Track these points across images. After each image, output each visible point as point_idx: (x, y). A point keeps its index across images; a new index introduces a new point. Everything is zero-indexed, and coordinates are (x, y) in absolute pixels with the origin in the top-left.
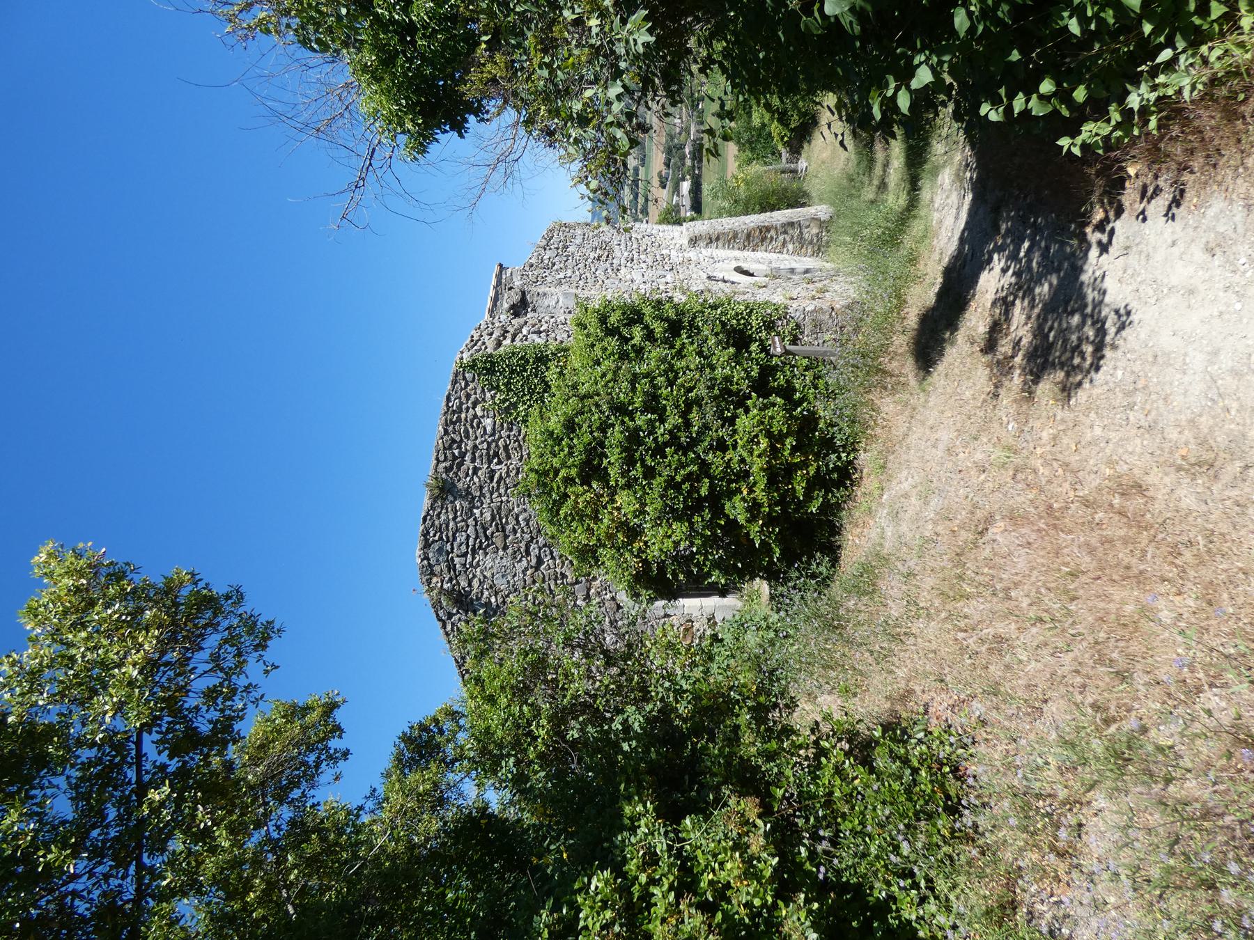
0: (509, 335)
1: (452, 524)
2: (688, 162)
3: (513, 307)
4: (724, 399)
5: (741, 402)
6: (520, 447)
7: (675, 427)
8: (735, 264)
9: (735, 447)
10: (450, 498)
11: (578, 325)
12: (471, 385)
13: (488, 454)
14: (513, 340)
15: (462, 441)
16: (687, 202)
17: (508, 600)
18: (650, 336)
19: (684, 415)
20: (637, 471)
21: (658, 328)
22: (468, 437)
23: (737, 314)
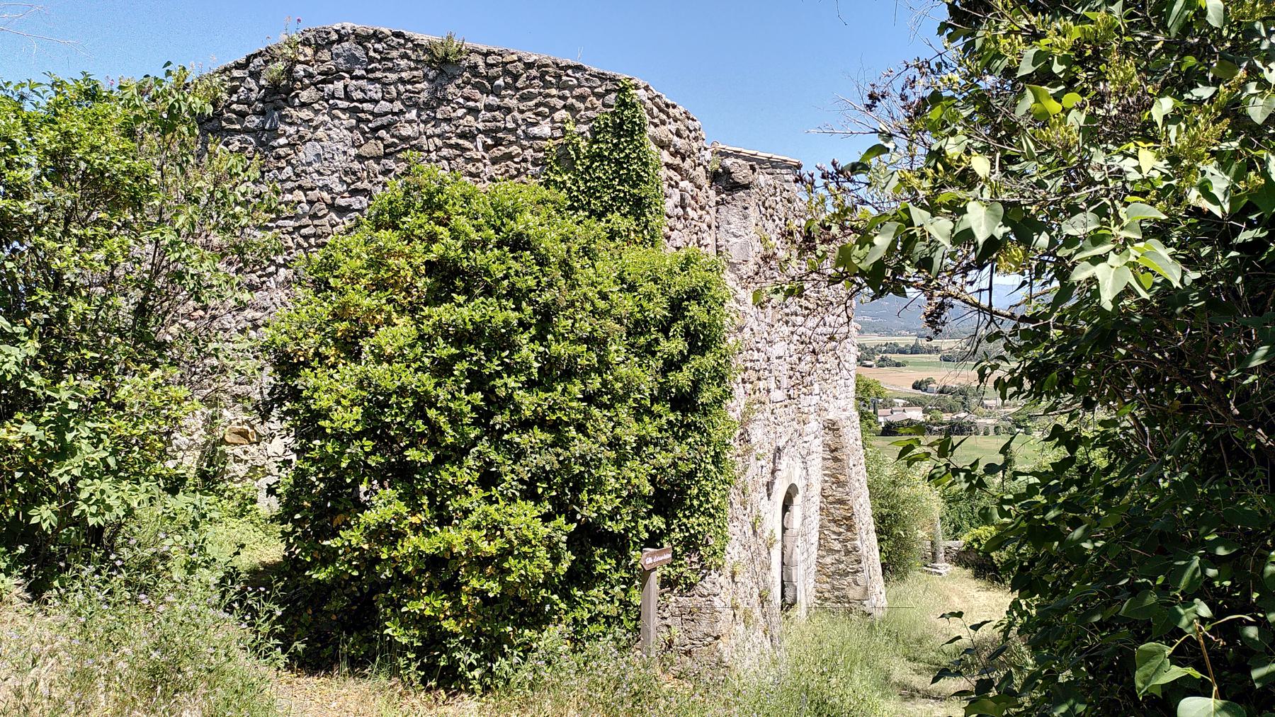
0: (678, 161)
1: (393, 77)
2: (946, 417)
3: (727, 172)
4: (567, 481)
5: (561, 507)
6: (512, 177)
7: (517, 409)
8: (800, 485)
9: (490, 500)
10: (432, 74)
11: (688, 259)
12: (598, 103)
13: (498, 130)
14: (668, 166)
15: (517, 89)
16: (896, 417)
17: (283, 163)
18: (671, 365)
19: (539, 421)
20: (445, 350)
21: (682, 378)
22: (523, 98)
23: (706, 494)
